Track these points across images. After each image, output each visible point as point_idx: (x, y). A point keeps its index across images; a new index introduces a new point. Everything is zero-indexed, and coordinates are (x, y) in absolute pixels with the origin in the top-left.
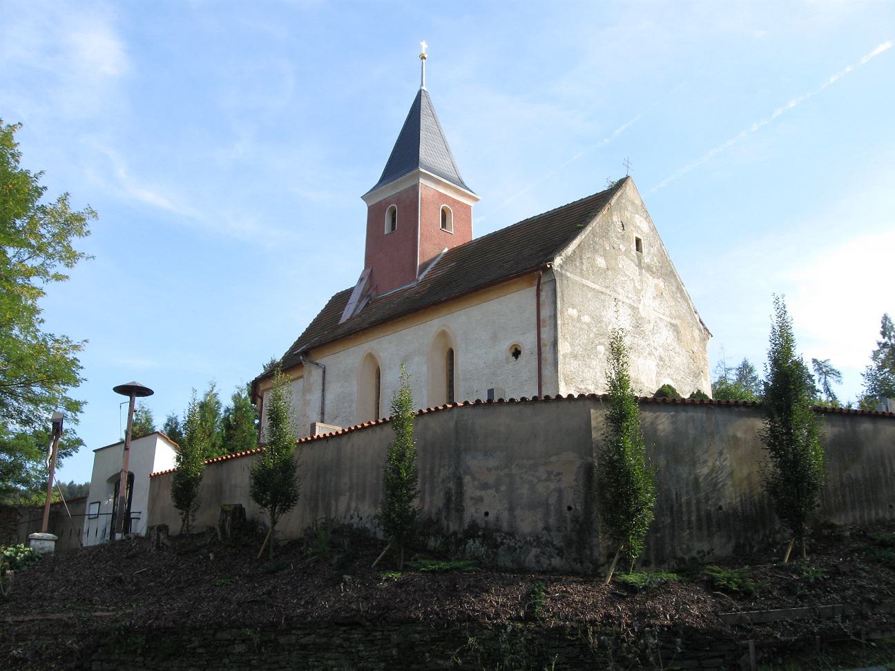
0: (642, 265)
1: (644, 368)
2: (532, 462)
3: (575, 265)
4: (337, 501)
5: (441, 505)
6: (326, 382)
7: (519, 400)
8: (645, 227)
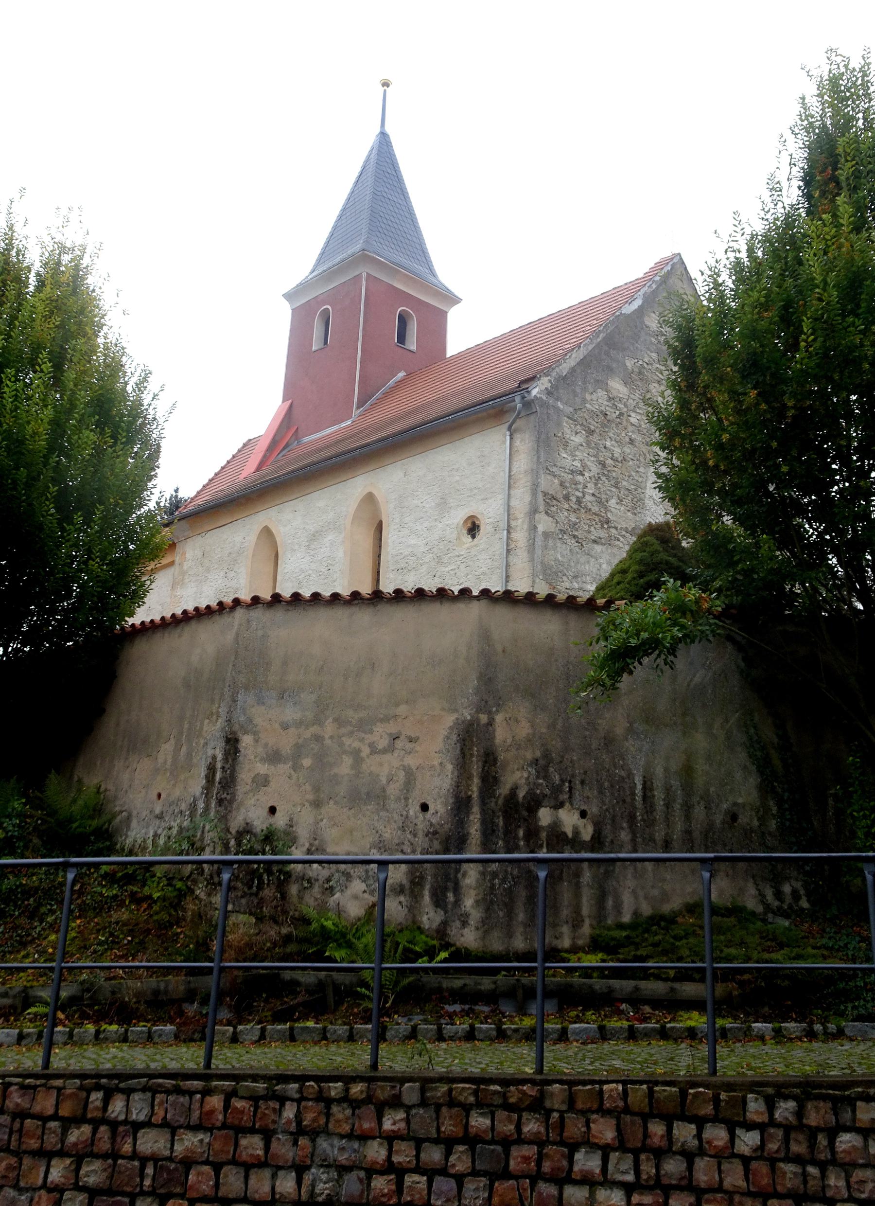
7: (456, 593)
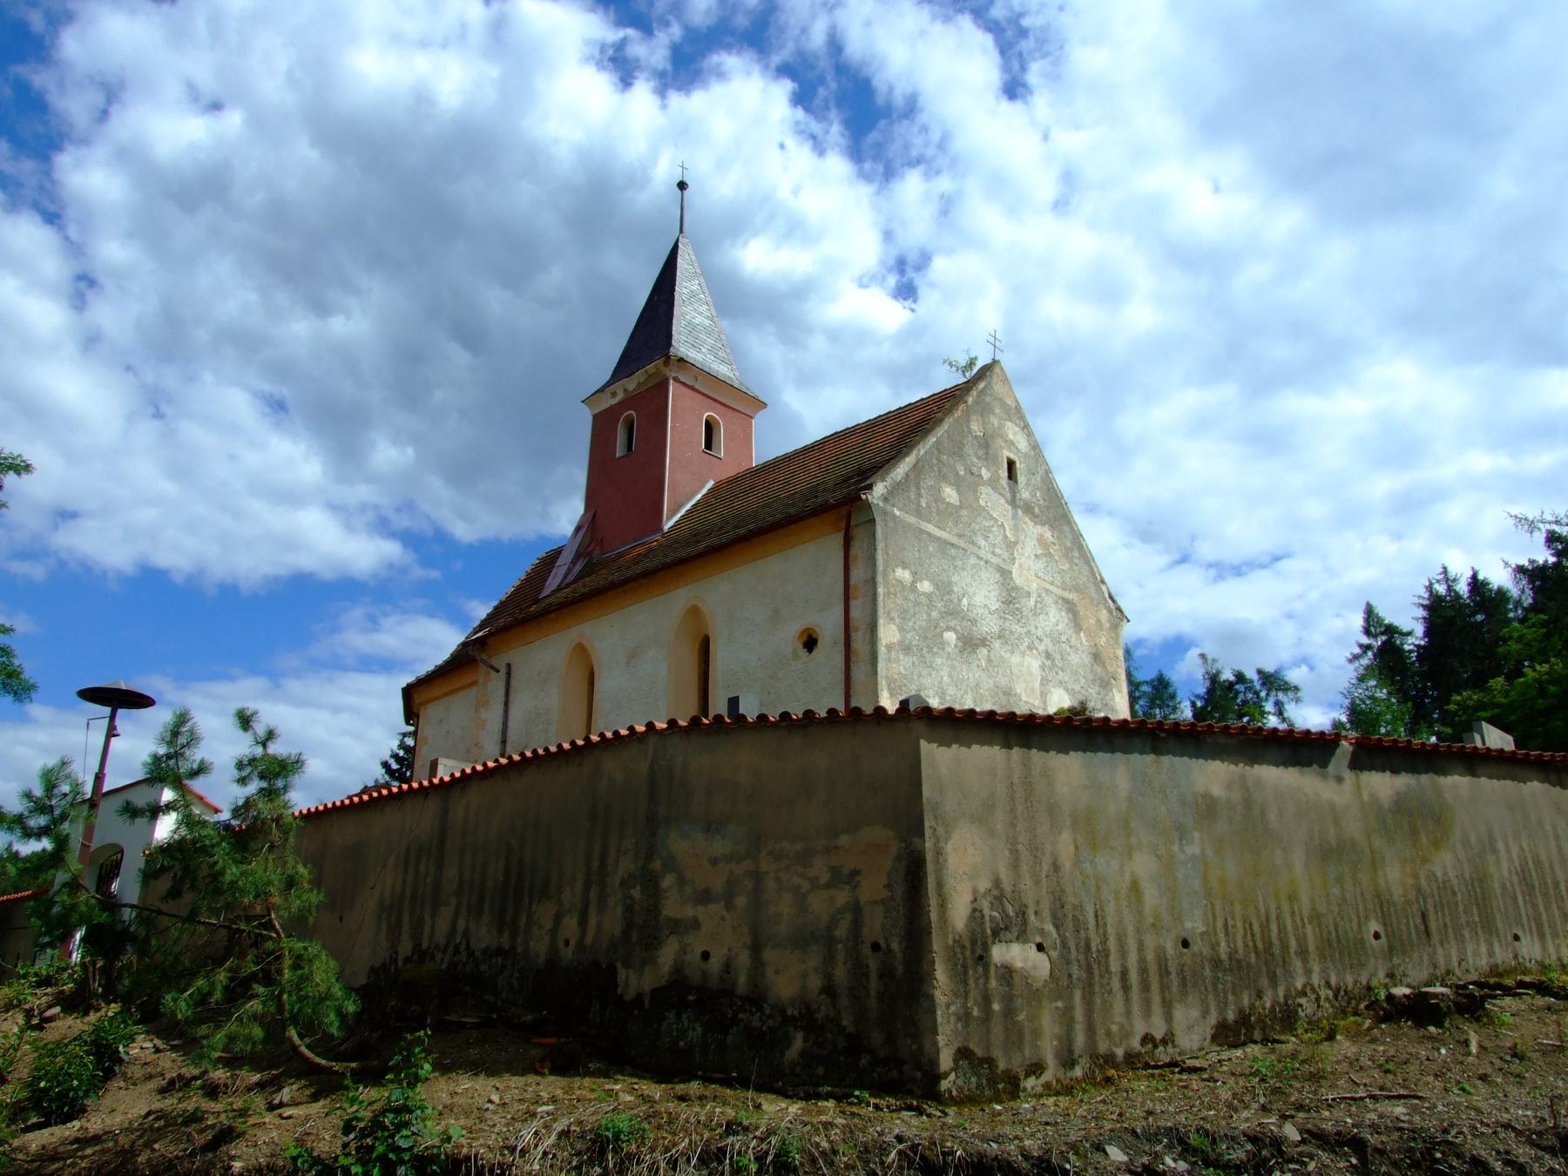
0: (1018, 502)
1: (1020, 671)
2: (799, 846)
3: (909, 497)
4: (433, 916)
5: (618, 931)
6: (511, 690)
8: (1022, 443)
